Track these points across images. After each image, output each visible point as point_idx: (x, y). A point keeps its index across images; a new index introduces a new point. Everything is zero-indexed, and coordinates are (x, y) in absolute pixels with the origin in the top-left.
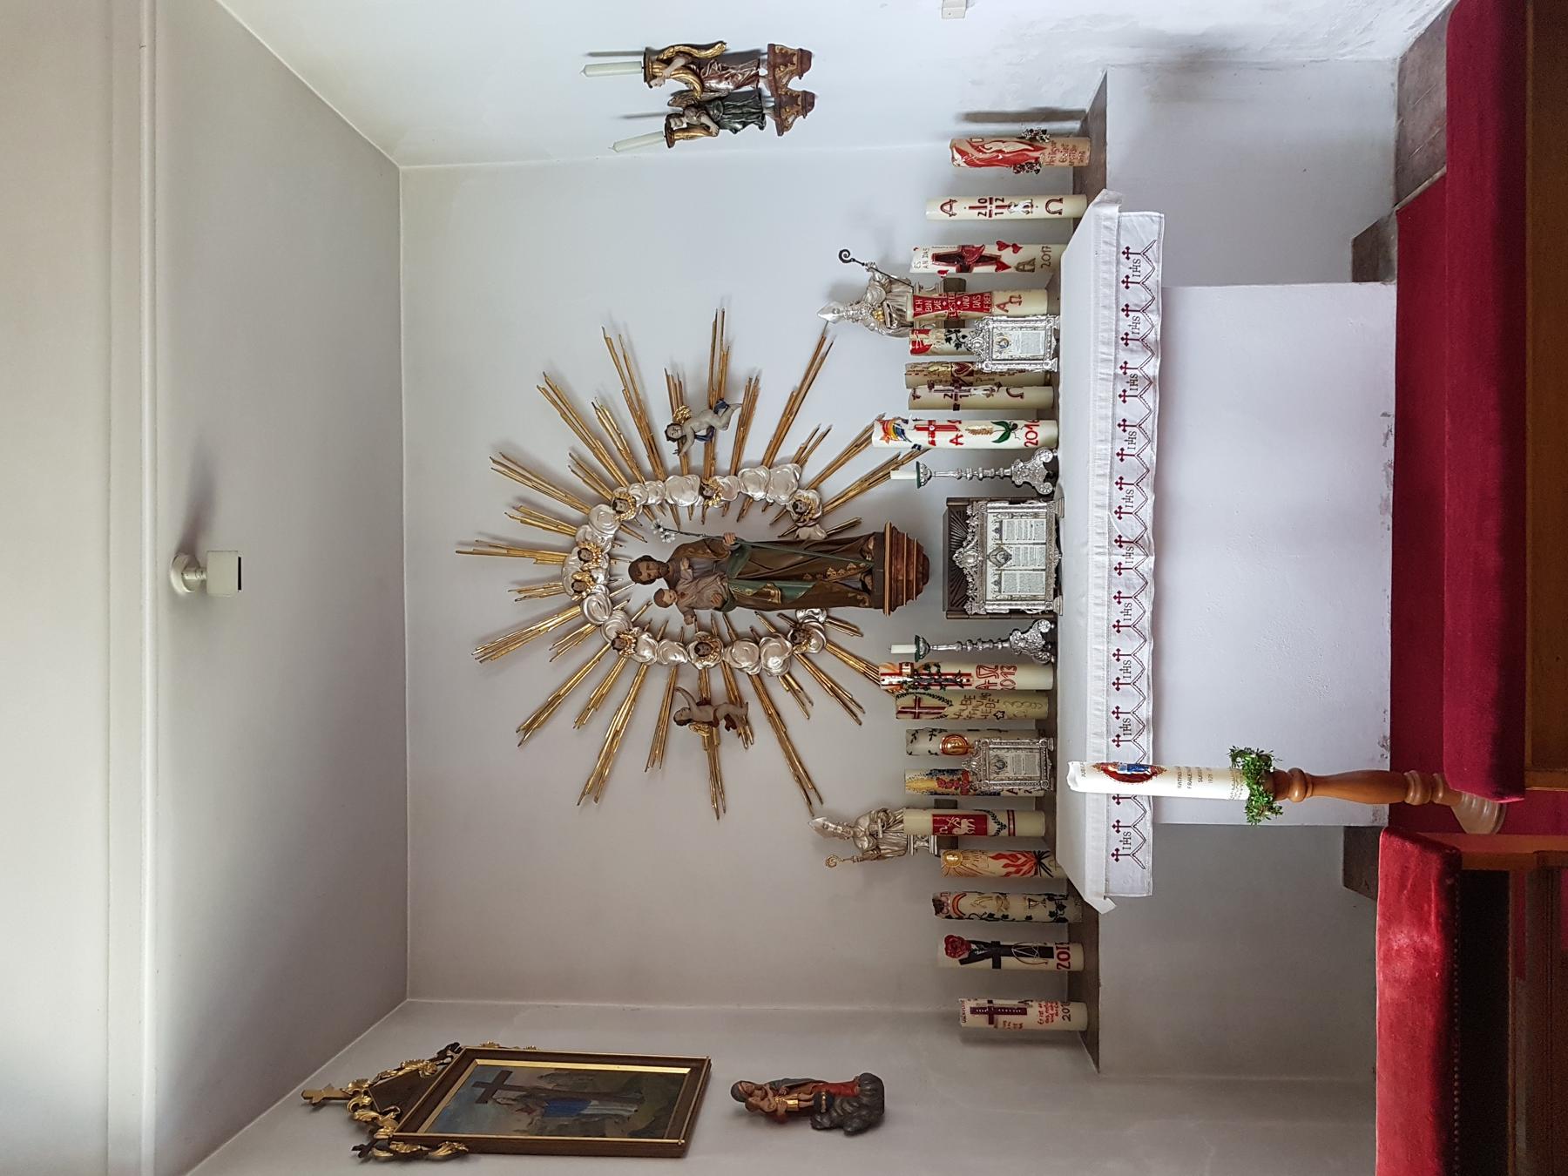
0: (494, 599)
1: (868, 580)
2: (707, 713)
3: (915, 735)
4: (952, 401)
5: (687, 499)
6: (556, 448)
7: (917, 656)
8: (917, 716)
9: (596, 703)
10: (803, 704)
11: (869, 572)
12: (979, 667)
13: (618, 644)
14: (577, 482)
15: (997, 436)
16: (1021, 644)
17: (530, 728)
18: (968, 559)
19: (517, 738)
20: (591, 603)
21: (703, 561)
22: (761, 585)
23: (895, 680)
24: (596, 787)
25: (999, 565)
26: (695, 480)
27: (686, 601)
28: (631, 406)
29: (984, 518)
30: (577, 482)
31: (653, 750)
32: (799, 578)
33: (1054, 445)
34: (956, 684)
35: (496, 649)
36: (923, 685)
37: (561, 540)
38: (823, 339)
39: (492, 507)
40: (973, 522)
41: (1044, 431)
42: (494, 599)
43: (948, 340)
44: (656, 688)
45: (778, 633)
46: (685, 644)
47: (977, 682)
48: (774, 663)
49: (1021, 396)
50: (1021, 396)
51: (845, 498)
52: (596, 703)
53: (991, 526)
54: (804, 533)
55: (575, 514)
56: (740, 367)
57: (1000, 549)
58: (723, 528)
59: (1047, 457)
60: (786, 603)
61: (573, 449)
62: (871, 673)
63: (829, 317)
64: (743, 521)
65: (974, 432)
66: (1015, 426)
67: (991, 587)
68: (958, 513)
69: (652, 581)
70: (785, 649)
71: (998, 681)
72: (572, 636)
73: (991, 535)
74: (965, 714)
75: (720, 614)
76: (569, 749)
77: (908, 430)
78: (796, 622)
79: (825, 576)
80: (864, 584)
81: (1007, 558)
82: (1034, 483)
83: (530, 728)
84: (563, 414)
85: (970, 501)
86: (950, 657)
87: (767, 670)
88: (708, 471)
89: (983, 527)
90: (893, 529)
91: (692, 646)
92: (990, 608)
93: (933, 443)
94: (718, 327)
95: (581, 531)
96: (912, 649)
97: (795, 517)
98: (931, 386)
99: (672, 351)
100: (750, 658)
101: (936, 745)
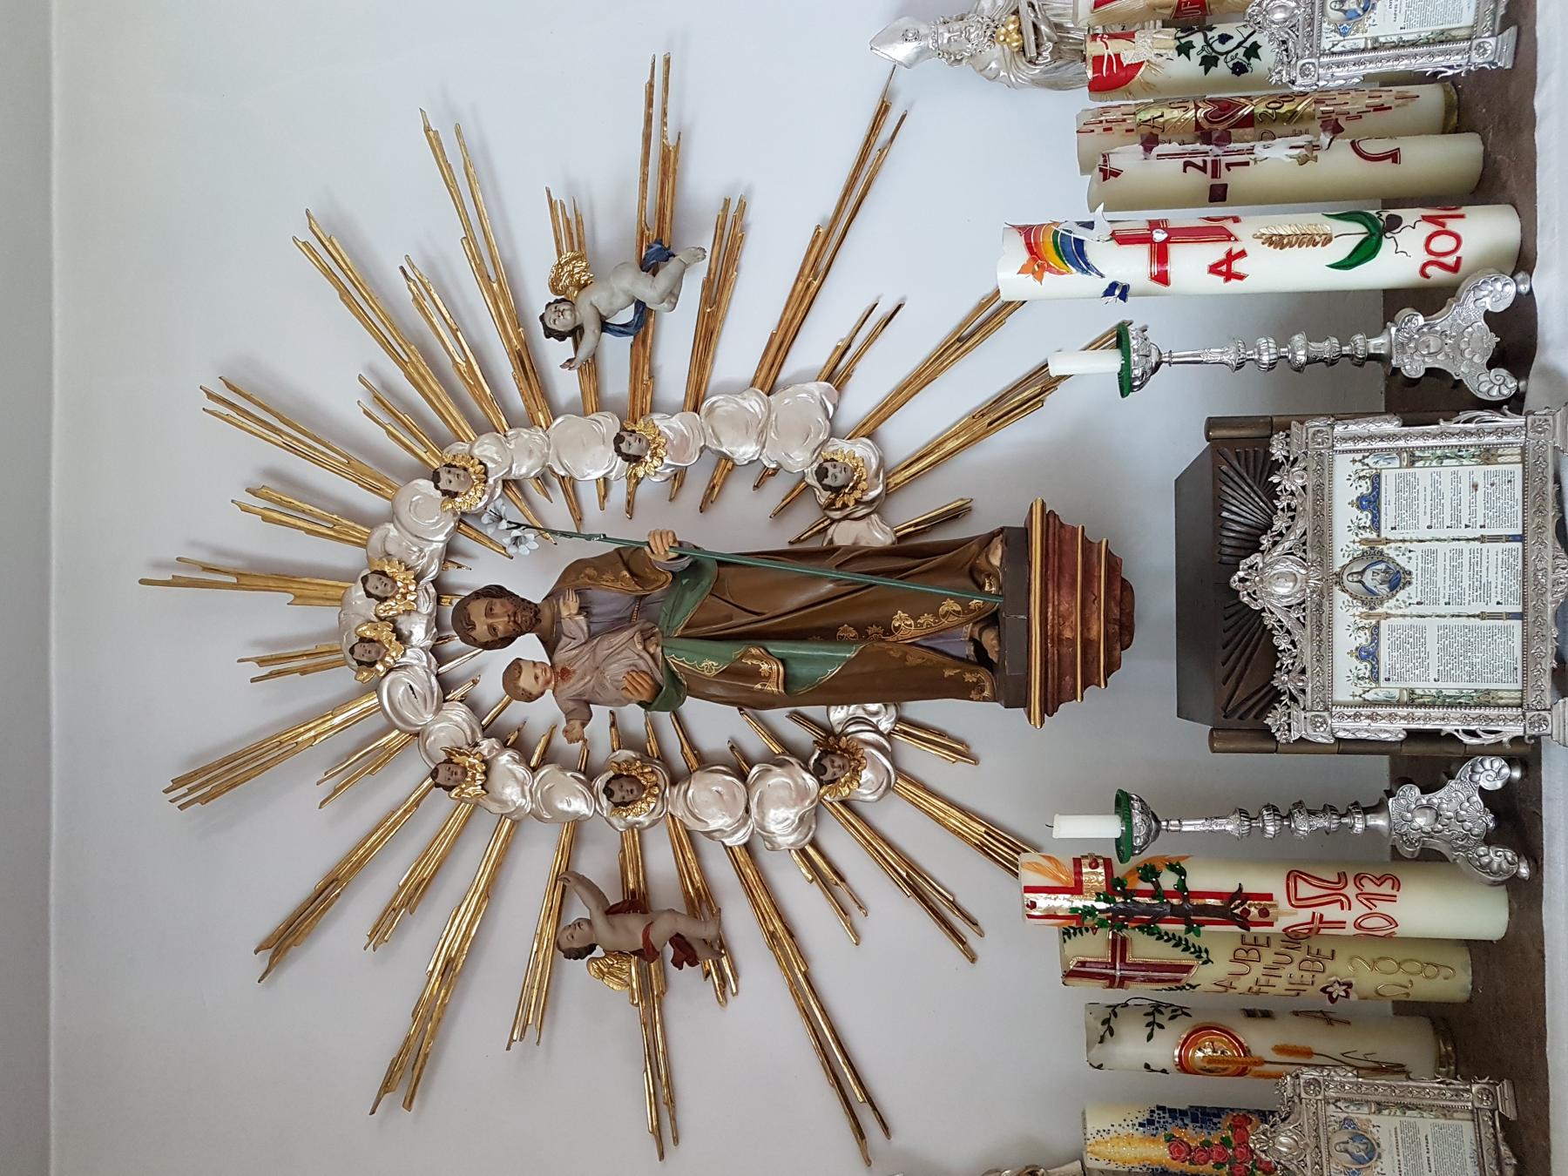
0: (207, 677)
1: (989, 639)
2: (632, 929)
3: (1108, 1023)
4: (1205, 180)
5: (596, 464)
6: (334, 368)
7: (1124, 846)
8: (1112, 982)
9: (415, 894)
10: (844, 911)
11: (992, 620)
12: (1293, 876)
13: (448, 773)
14: (376, 435)
15: (1343, 247)
16: (1420, 821)
17: (284, 941)
18: (1275, 583)
19: (261, 962)
20: (396, 688)
21: (611, 596)
22: (734, 651)
23: (1063, 903)
24: (409, 1072)
25: (1370, 599)
26: (609, 425)
27: (574, 686)
28: (480, 269)
29: (1323, 468)
30: (376, 435)
31: (523, 1004)
32: (828, 635)
33: (1523, 261)
34: (1230, 919)
35: (215, 779)
36: (1136, 914)
37: (345, 557)
38: (883, 110)
39: (209, 490)
40: (1290, 481)
41: (1484, 230)
42: (207, 677)
43: (1184, 49)
44: (535, 865)
45: (787, 754)
46: (589, 774)
47: (1288, 917)
48: (781, 821)
49: (1394, 156)
50: (1394, 156)
51: (934, 457)
52: (415, 894)
53: (1345, 488)
54: (844, 534)
55: (372, 503)
56: (705, 183)
57: (1372, 554)
58: (667, 524)
59: (1499, 294)
60: (794, 692)
61: (372, 370)
62: (1003, 847)
63: (903, 51)
64: (715, 512)
65: (1277, 242)
66: (1394, 223)
67: (1345, 666)
68: (1240, 469)
69: (507, 641)
70: (803, 792)
71: (1349, 916)
72: (367, 759)
73: (1345, 520)
74: (1243, 984)
75: (665, 717)
76: (357, 992)
77: (1099, 251)
78: (828, 731)
79: (889, 631)
80: (979, 646)
81: (1397, 580)
82: (1461, 371)
83: (284, 941)
84: (344, 294)
85: (1275, 425)
86: (1219, 850)
87: (769, 838)
88: (643, 398)
89: (1321, 495)
90: (1049, 517)
91: (600, 783)
92: (1346, 728)
93: (1162, 278)
94: (656, 96)
95: (378, 534)
96: (1108, 828)
97: (824, 497)
98: (1149, 142)
99: (568, 159)
100: (728, 810)
101: (1164, 1049)
